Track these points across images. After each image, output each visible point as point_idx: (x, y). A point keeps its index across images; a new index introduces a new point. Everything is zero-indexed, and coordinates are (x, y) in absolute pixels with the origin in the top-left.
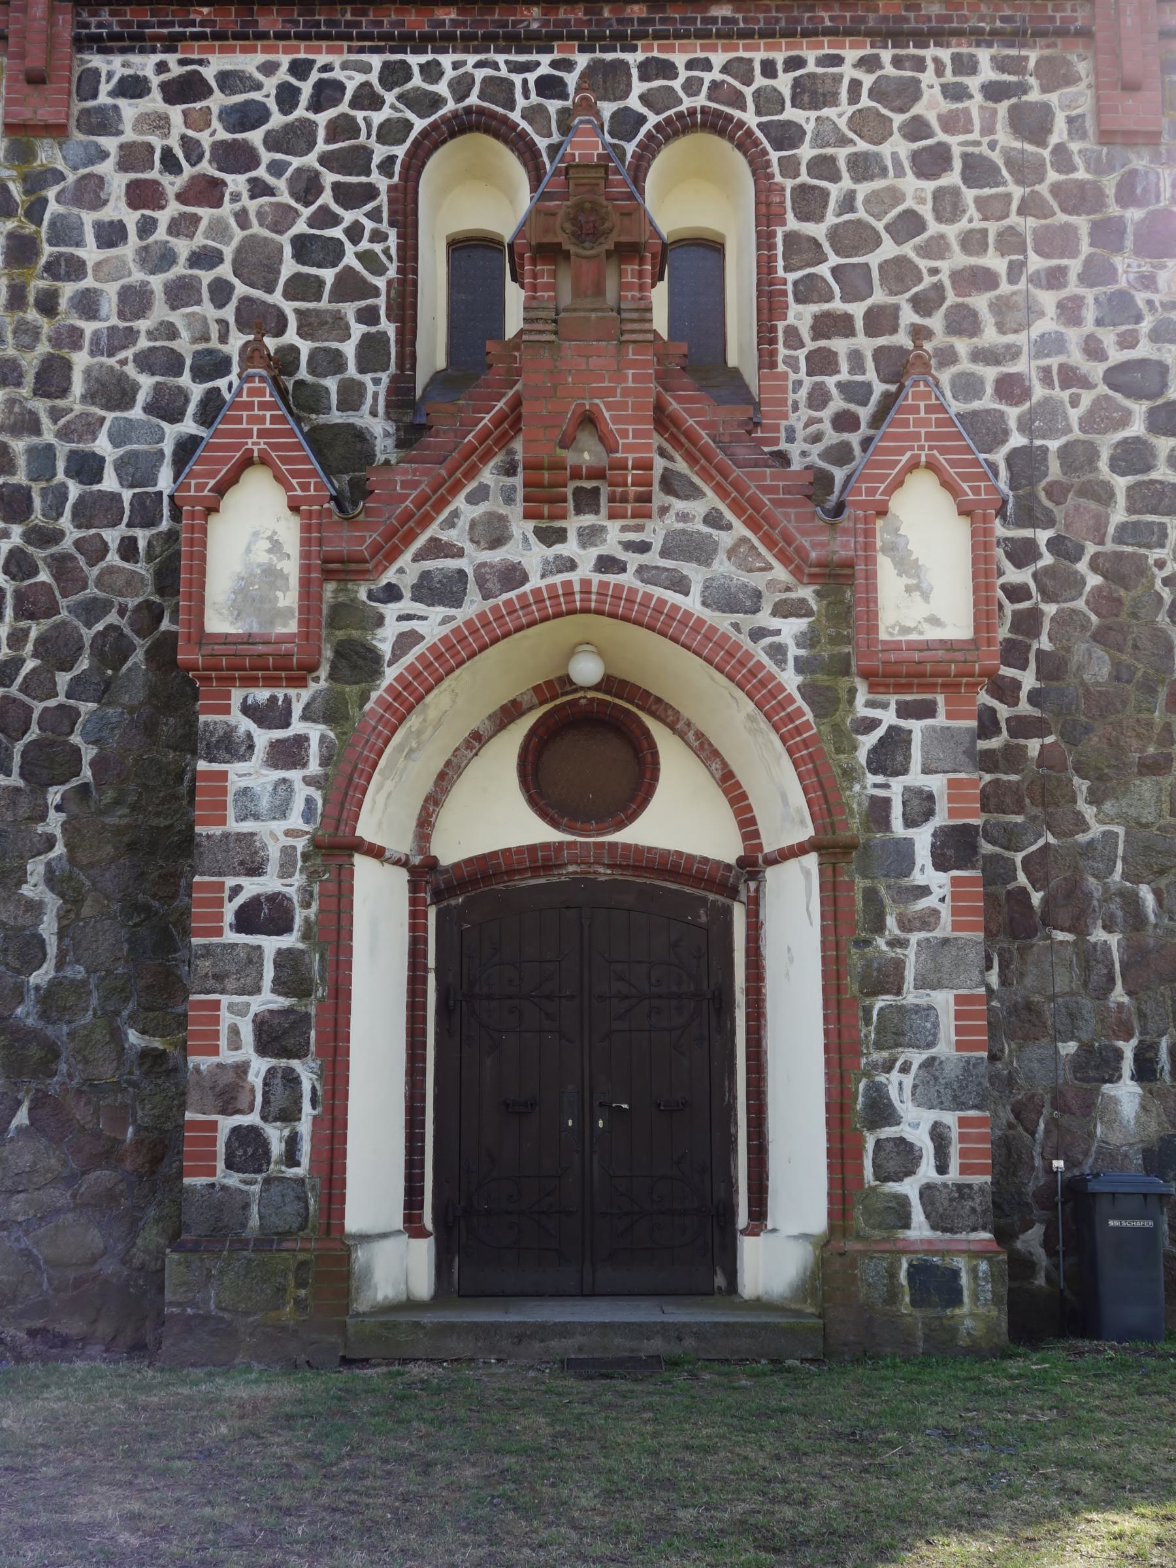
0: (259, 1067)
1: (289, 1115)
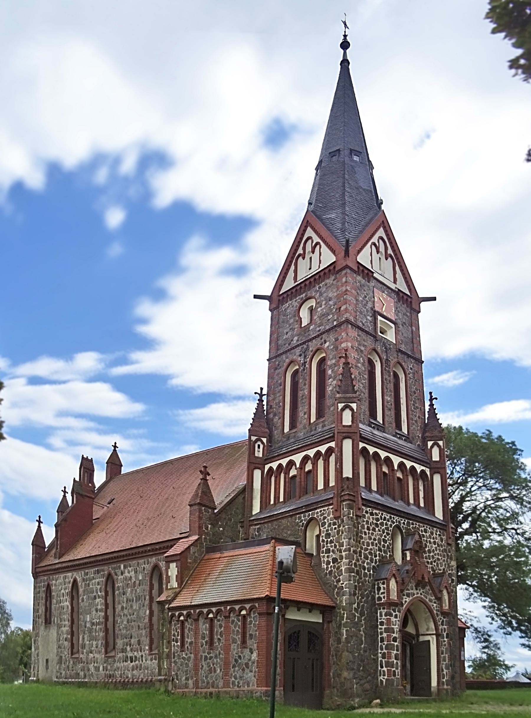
0: (395, 661)
1: (397, 669)
